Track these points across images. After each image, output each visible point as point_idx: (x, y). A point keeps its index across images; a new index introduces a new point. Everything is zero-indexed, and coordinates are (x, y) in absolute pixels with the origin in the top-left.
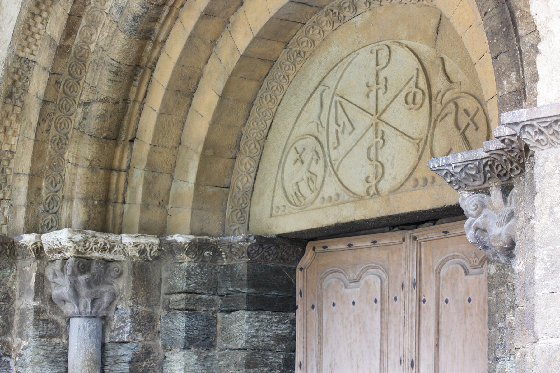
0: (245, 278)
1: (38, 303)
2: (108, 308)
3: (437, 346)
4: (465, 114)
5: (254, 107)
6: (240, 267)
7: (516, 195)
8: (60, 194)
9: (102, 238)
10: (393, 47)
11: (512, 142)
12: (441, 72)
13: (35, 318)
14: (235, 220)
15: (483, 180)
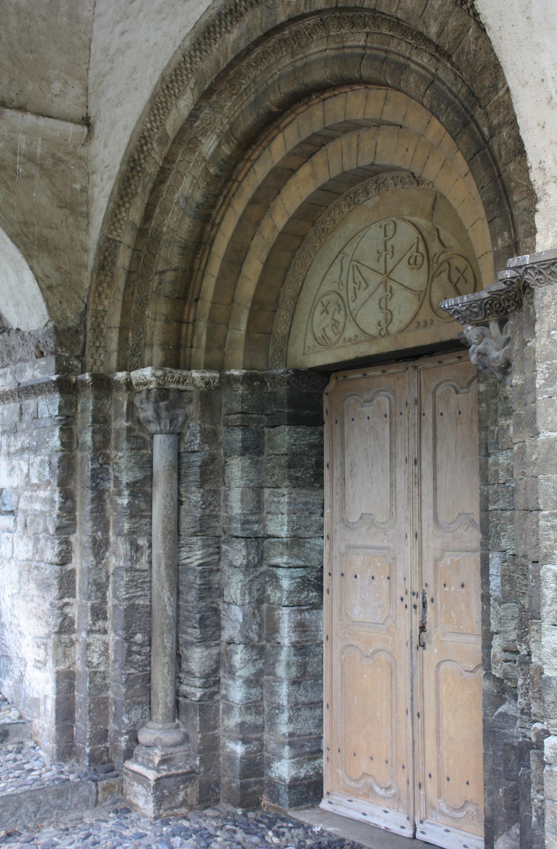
0: (286, 401)
1: (129, 424)
2: (182, 427)
3: (435, 448)
4: (456, 271)
5: (289, 272)
6: (281, 393)
7: (512, 325)
8: (143, 342)
9: (177, 373)
10: (398, 222)
11: (513, 283)
12: (437, 240)
13: (127, 435)
14: (276, 357)
15: (484, 315)
